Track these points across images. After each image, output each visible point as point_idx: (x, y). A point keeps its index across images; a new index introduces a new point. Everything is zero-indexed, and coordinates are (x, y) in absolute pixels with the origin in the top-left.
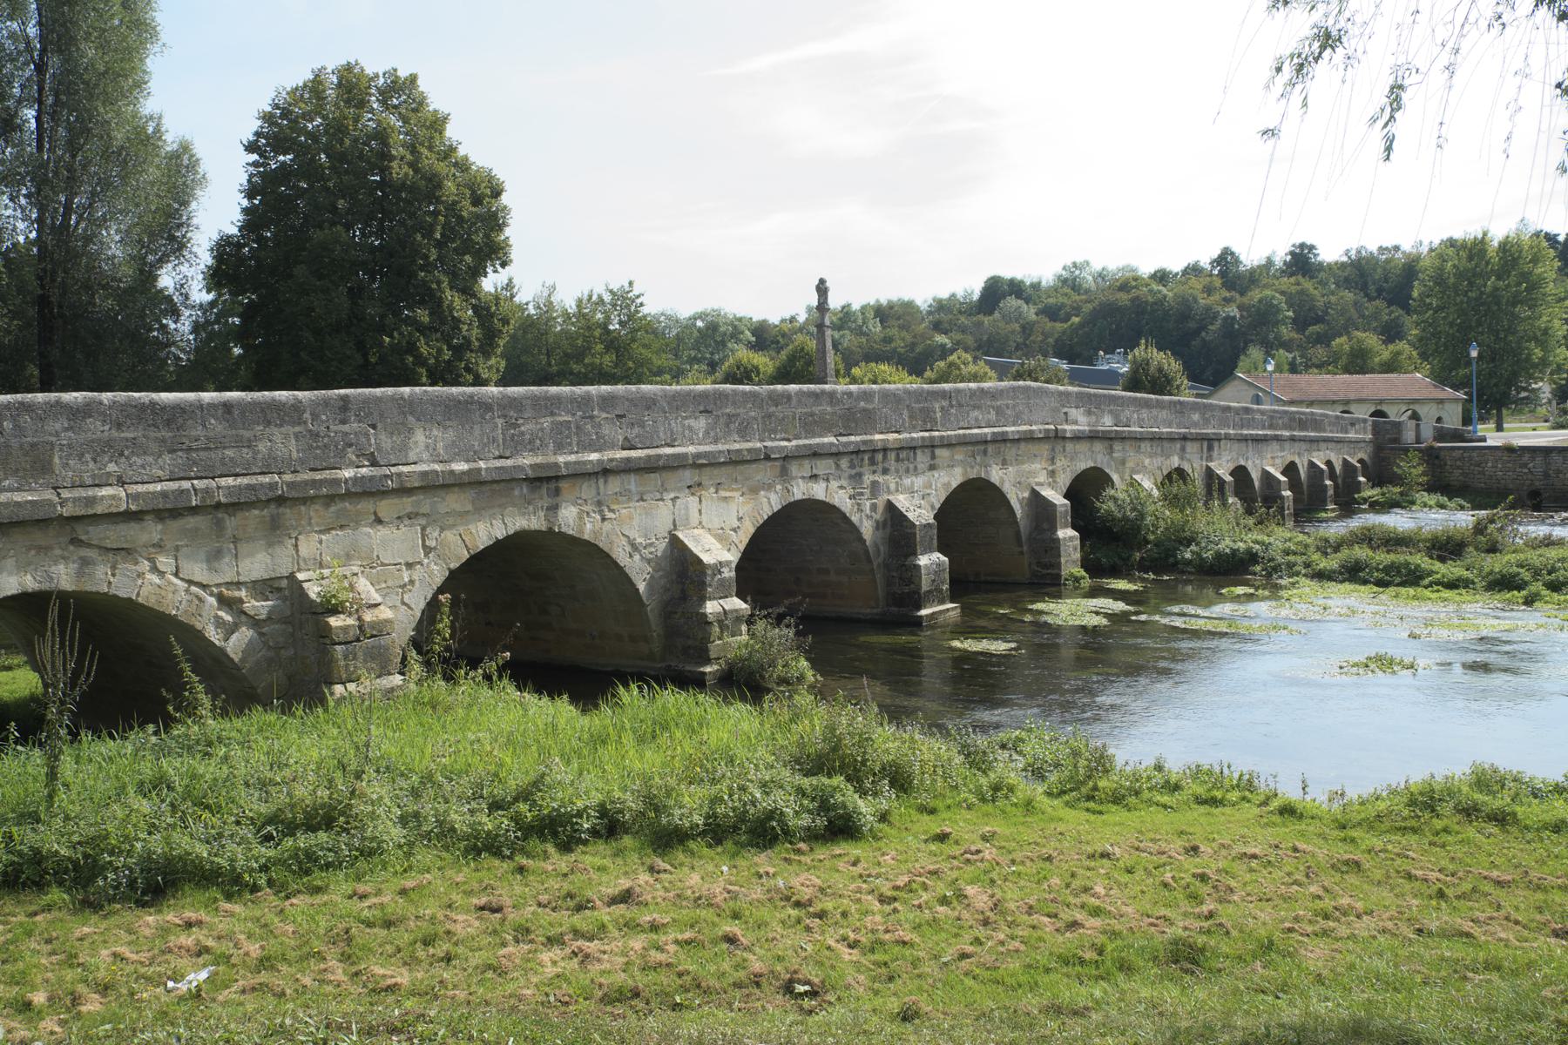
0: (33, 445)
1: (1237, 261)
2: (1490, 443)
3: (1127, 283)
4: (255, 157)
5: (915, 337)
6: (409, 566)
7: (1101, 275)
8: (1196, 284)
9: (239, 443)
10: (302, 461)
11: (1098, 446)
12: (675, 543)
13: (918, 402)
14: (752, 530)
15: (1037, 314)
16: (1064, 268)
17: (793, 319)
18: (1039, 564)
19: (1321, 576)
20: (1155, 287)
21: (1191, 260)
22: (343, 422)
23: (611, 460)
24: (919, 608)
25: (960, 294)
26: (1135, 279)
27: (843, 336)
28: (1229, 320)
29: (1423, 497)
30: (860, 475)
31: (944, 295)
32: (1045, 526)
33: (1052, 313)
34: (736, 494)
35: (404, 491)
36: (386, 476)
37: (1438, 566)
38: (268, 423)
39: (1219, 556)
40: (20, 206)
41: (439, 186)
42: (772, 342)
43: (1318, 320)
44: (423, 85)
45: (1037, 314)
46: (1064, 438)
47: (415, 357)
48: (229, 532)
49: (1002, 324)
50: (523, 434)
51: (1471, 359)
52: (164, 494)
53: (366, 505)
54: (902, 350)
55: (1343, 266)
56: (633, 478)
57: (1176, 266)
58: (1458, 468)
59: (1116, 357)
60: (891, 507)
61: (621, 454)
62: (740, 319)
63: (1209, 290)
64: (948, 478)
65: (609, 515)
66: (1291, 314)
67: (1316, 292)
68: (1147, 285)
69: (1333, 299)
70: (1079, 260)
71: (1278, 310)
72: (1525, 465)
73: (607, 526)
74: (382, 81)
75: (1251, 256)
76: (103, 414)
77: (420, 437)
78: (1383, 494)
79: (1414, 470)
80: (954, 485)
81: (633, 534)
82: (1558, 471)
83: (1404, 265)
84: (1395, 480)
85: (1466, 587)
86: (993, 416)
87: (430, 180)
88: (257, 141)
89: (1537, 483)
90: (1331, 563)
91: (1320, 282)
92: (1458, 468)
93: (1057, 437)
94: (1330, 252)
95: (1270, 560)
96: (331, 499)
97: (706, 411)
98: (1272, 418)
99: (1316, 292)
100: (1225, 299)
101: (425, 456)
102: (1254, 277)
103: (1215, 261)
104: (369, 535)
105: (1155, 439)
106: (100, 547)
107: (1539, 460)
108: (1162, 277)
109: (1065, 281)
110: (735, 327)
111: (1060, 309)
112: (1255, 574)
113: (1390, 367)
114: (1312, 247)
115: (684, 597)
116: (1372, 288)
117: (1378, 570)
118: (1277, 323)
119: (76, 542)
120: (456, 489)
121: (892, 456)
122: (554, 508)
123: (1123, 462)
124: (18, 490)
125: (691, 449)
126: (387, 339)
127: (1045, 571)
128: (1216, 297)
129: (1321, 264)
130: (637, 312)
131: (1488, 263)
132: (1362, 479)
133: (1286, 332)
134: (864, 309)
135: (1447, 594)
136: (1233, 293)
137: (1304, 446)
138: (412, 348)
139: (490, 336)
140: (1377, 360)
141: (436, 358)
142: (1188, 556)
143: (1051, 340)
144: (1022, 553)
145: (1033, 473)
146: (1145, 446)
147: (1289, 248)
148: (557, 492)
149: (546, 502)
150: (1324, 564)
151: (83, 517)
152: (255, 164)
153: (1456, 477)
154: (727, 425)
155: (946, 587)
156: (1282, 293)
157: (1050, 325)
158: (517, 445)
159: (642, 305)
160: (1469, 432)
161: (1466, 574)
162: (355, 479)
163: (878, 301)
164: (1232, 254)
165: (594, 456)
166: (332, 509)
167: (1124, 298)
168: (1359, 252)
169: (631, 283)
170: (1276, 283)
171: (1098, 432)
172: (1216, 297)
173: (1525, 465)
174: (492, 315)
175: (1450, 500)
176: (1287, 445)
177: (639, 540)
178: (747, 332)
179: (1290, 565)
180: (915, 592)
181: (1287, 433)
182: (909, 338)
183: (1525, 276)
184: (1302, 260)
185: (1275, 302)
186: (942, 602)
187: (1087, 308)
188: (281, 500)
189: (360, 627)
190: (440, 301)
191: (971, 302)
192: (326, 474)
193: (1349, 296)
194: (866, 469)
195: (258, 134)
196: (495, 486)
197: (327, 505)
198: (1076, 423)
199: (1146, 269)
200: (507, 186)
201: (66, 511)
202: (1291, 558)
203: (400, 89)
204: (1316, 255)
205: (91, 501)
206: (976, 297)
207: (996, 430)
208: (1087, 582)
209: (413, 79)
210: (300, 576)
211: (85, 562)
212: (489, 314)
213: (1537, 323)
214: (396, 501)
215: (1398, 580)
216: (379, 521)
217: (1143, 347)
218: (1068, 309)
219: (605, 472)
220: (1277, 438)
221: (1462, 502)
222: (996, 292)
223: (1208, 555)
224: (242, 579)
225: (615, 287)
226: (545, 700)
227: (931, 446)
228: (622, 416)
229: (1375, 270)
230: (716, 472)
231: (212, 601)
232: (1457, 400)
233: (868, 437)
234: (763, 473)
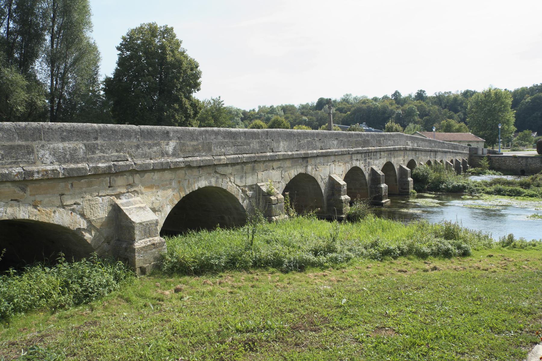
0: (208, 143)
1: (400, 95)
2: (504, 155)
3: (365, 102)
4: (119, 52)
5: (296, 117)
6: (279, 182)
7: (355, 99)
8: (387, 103)
9: (249, 144)
10: (259, 150)
11: (414, 153)
12: (330, 178)
13: (378, 138)
14: (345, 175)
15: (336, 111)
16: (344, 96)
17: (254, 110)
18: (402, 188)
19: (488, 193)
20: (374, 103)
21: (385, 94)
22: (267, 139)
23: (319, 153)
24: (382, 200)
25: (310, 104)
26: (368, 100)
27: (272, 116)
28: (399, 114)
29: (487, 171)
30: (366, 159)
31: (304, 103)
32: (404, 177)
33: (340, 110)
34: (342, 164)
35: (279, 160)
36: (276, 155)
37: (525, 191)
38: (253, 138)
39: (454, 187)
41: (181, 64)
42: (248, 118)
43: (426, 115)
44: (175, 31)
45: (336, 111)
46: (407, 150)
47: (174, 119)
48: (244, 171)
49: (324, 114)
50: (301, 144)
51: (499, 129)
52: (233, 158)
53: (271, 164)
54: (292, 121)
55: (434, 98)
56: (322, 158)
57: (380, 96)
58: (497, 162)
59: (363, 125)
60: (372, 169)
61: (321, 151)
62: (239, 110)
63: (391, 104)
64: (383, 161)
65: (317, 169)
66: (418, 113)
67: (426, 106)
68: (371, 102)
69: (431, 108)
70: (348, 93)
71: (415, 111)
72: (519, 162)
73: (317, 172)
74: (162, 28)
75: (404, 94)
76: (221, 134)
77: (281, 144)
78: (475, 170)
79: (485, 162)
80: (384, 163)
81: (322, 175)
82: (530, 164)
83: (454, 98)
84: (480, 166)
85: (536, 197)
86: (393, 143)
87: (179, 62)
88: (121, 47)
89: (523, 168)
90: (492, 189)
91: (427, 103)
92: (497, 162)
93: (406, 150)
94: (430, 93)
95: (470, 189)
96: (265, 161)
97: (337, 139)
98: (448, 145)
99: (426, 106)
100: (397, 107)
101: (283, 150)
102: (405, 101)
103: (393, 95)
104: (271, 173)
105: (425, 151)
106: (220, 174)
107: (524, 160)
108: (375, 99)
109: (344, 100)
110: (237, 112)
111: (343, 109)
112: (466, 192)
113: (458, 131)
114: (424, 91)
115: (333, 194)
116: (443, 105)
117: (507, 192)
118: (414, 116)
119: (216, 172)
121: (372, 154)
122: (307, 166)
123: (418, 158)
124: (205, 156)
125: (334, 150)
126: (166, 114)
127: (404, 191)
128: (394, 107)
129: (427, 97)
130: (221, 106)
131: (491, 98)
132: (468, 165)
133: (417, 118)
134: (277, 107)
135: (531, 198)
136: (399, 105)
137: (454, 154)
138: (173, 116)
139: (196, 113)
140: (454, 128)
141: (181, 120)
142: (443, 187)
143: (341, 119)
144: (397, 185)
145: (400, 161)
146: (423, 153)
147: (417, 91)
148: (307, 162)
149: (305, 165)
150: (488, 189)
151: (219, 164)
152: (119, 54)
153: (496, 165)
154: (341, 143)
155: (387, 194)
156: (416, 106)
157: (340, 114)
158: (300, 147)
159: (223, 104)
160: (497, 151)
161: (535, 193)
162: (271, 156)
163: (282, 105)
164: (399, 93)
165: (315, 151)
166: (265, 165)
167: (364, 106)
168: (439, 93)
169: (220, 97)
170: (413, 102)
172: (394, 107)
173: (519, 162)
174: (197, 107)
175: (497, 172)
176: (451, 154)
177: (323, 177)
178: (241, 114)
179: (478, 190)
180: (380, 196)
181: (451, 150)
182: (294, 117)
183: (502, 103)
184: (420, 96)
185: (414, 109)
186: (386, 199)
187: (353, 109)
188: (255, 162)
189: (278, 200)
190: (181, 101)
191: (313, 106)
192: (263, 154)
193: (436, 107)
194: (367, 158)
195: (121, 44)
196: (296, 159)
197: (263, 163)
198: (409, 145)
199: (370, 97)
200: (200, 65)
201: (215, 163)
202: (478, 188)
203: (168, 32)
204: (425, 94)
205: (220, 160)
206: (315, 104)
207: (394, 147)
208: (416, 194)
209: (172, 29)
210: (259, 184)
211: (217, 178)
212: (195, 105)
213: (506, 118)
214: (277, 163)
215: (514, 194)
216: (273, 169)
217: (390, 122)
218: (346, 109)
219: (317, 156)
220: (449, 152)
221: (500, 173)
222: (322, 103)
223: (450, 186)
224: (247, 185)
225: (214, 98)
226: (329, 223)
227: (380, 151)
228: (320, 140)
229: (444, 99)
230: (338, 157)
231: (241, 191)
232: (482, 141)
233: (368, 148)
234: (347, 158)
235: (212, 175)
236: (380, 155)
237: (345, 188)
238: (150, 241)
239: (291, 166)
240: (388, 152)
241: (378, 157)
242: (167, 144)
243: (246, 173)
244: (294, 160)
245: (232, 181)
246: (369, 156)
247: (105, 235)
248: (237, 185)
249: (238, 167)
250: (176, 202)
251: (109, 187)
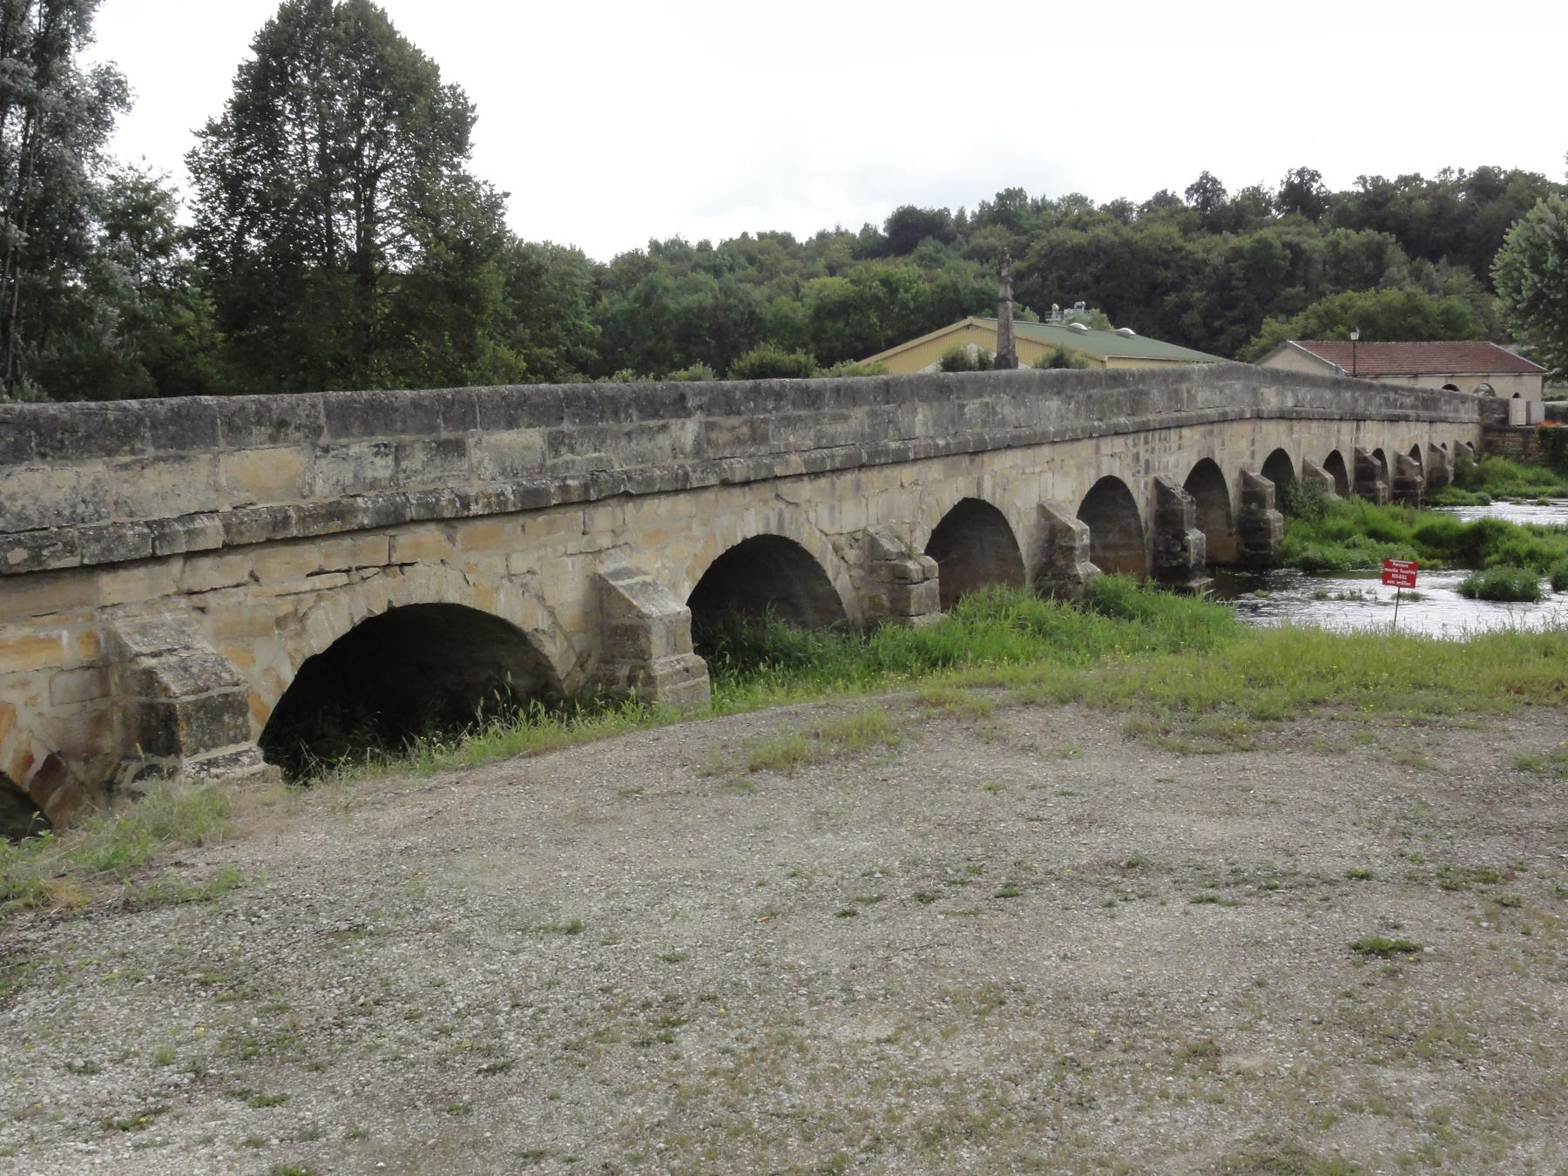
3: (1076, 212)
11: (1283, 426)
18: (1247, 545)
40: (388, 218)
94: (1338, 180)
108: (1119, 210)
114: (1315, 176)
120: (67, 575)
171: (1192, 417)
209: (1021, 190)
224: (844, 531)
235: (770, 504)
236: (1180, 438)
237: (1086, 541)
238: (678, 661)
239: (942, 477)
240: (1203, 428)
241: (1175, 446)
242: (682, 428)
243: (841, 499)
244: (949, 460)
245: (813, 520)
246: (1146, 443)
247: (577, 650)
248: (821, 531)
249: (824, 482)
250: (700, 575)
251: (584, 533)
